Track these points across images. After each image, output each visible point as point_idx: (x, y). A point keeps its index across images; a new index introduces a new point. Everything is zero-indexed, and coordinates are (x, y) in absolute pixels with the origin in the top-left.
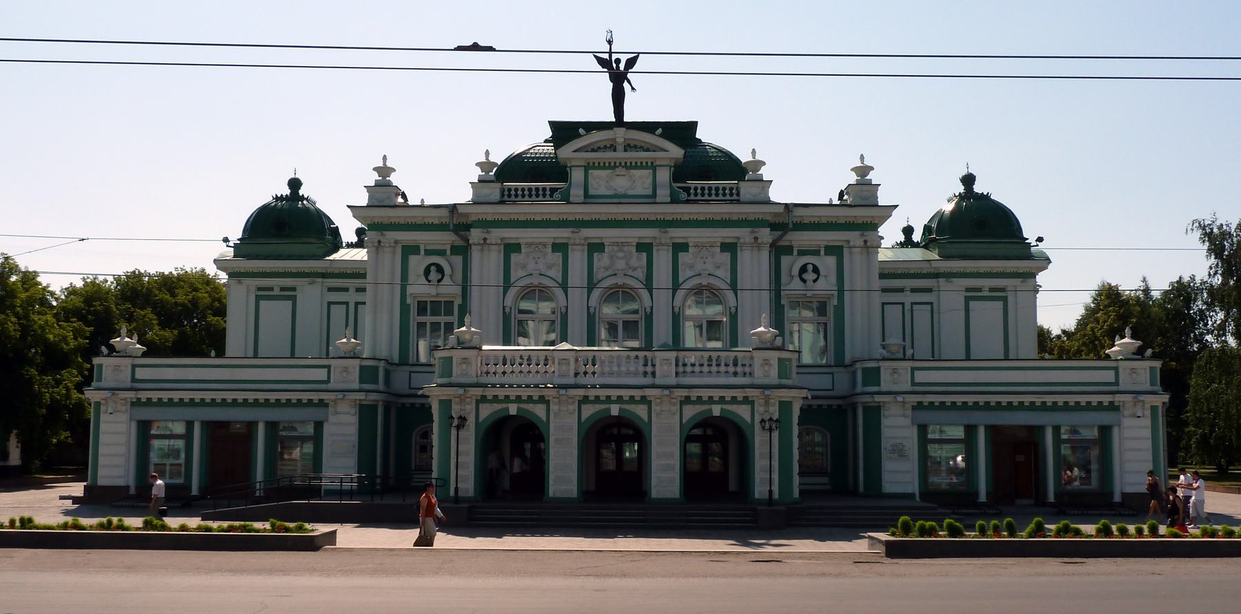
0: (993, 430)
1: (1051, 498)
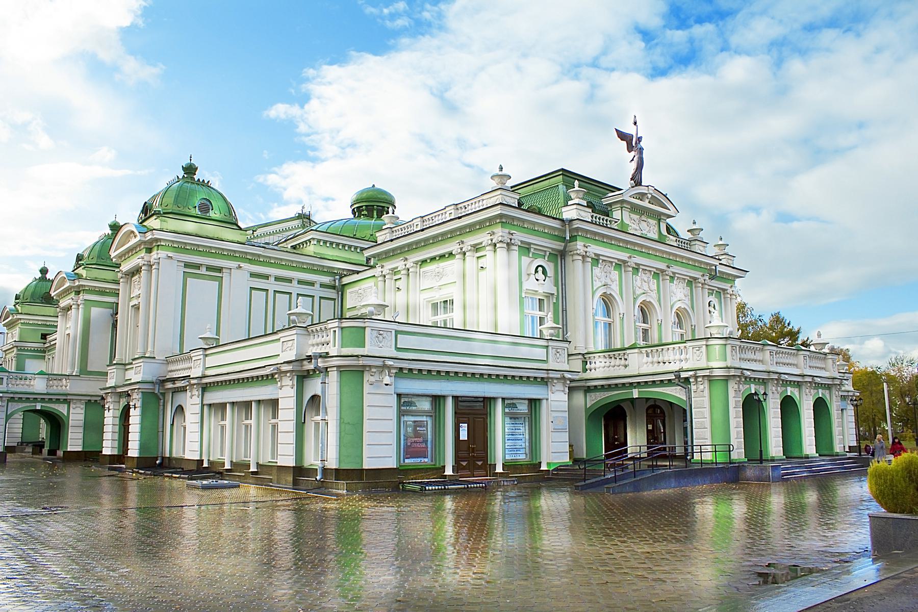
0: (455, 398)
1: (499, 469)
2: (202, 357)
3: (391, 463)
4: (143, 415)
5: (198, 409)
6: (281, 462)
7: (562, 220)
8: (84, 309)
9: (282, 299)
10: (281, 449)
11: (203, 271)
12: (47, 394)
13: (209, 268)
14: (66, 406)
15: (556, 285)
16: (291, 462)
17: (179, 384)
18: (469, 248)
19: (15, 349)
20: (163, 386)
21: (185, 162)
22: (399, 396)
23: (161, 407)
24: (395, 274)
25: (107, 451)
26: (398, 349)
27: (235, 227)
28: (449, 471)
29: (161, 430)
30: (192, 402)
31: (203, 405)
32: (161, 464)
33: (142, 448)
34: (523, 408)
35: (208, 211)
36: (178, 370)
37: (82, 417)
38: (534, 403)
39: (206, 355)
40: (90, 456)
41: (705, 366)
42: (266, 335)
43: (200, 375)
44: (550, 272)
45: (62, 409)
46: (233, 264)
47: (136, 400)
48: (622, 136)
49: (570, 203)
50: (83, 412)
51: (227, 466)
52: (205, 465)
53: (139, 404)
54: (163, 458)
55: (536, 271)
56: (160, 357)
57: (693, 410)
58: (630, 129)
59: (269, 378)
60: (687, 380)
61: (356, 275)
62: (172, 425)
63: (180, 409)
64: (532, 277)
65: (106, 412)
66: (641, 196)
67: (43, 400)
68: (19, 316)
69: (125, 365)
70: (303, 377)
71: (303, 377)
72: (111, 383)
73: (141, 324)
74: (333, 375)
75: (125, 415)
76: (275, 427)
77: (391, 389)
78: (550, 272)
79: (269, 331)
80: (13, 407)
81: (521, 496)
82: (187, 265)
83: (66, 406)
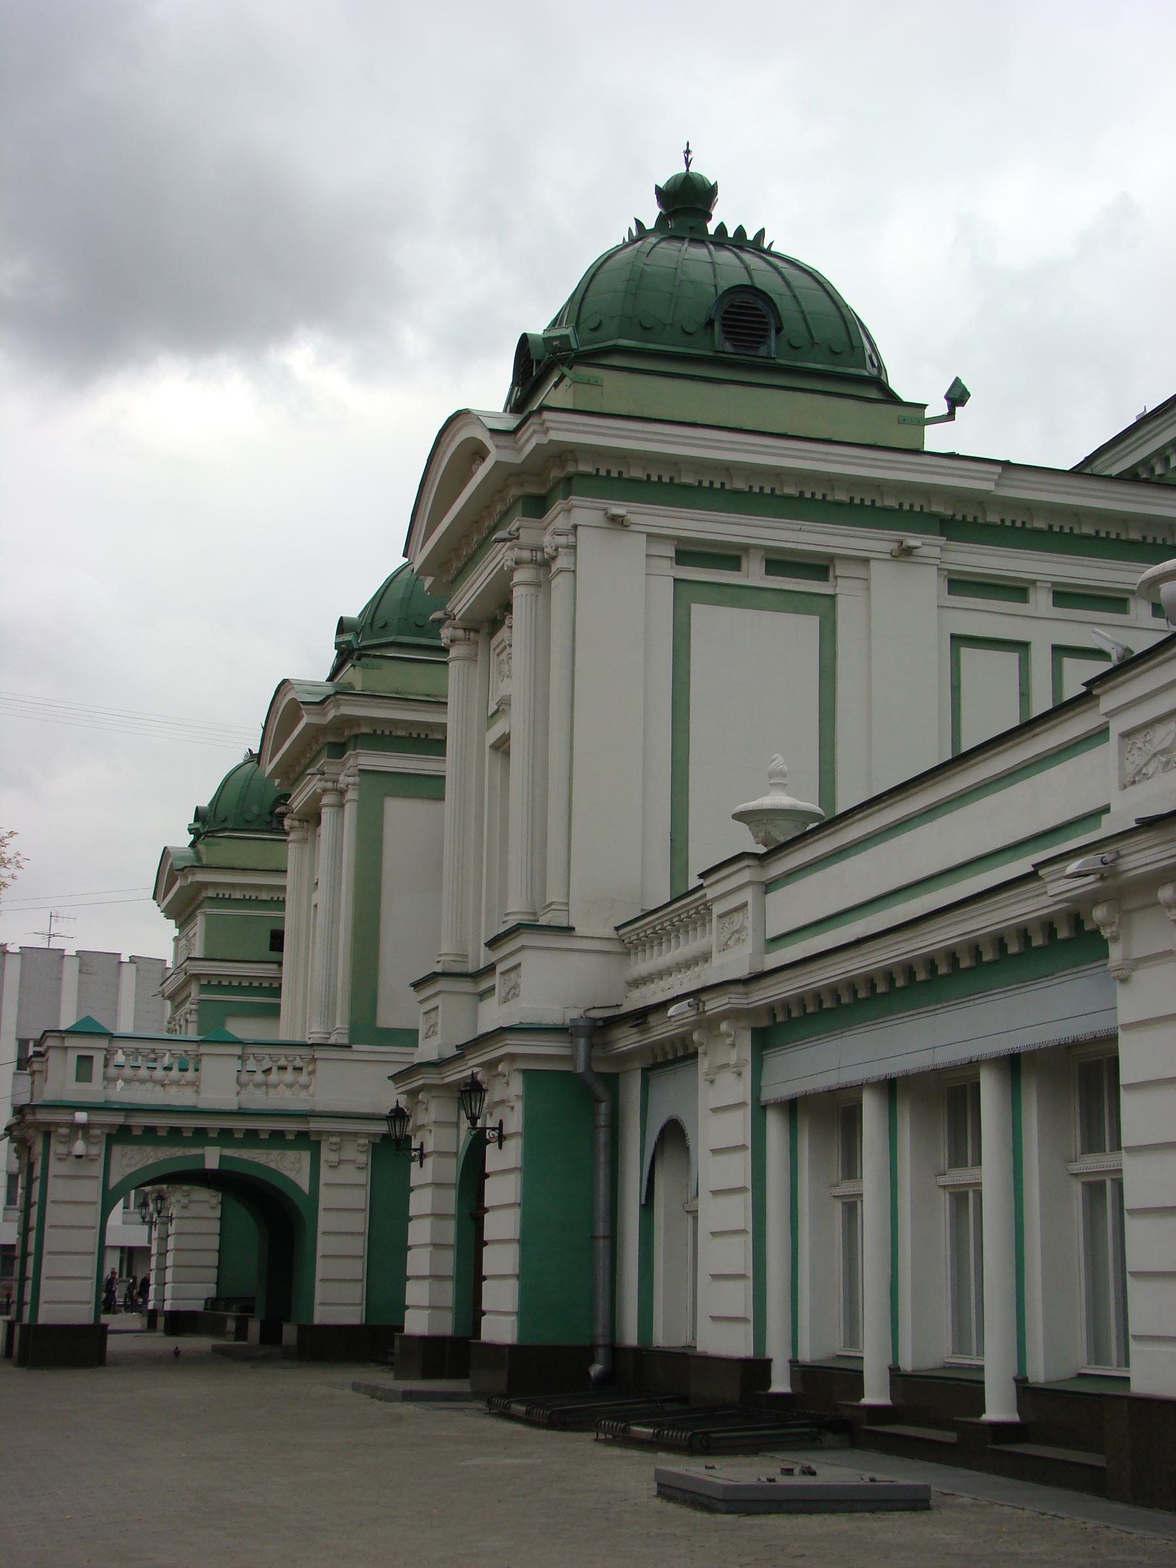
2: (747, 895)
4: (533, 1170)
5: (738, 1128)
8: (361, 803)
11: (753, 574)
12: (241, 1113)
13: (778, 563)
14: (306, 1156)
19: (194, 989)
20: (605, 1045)
21: (668, 170)
23: (602, 1136)
25: (416, 1323)
27: (874, 394)
29: (602, 1229)
30: (718, 1104)
31: (760, 1110)
32: (607, 1378)
33: (526, 1312)
35: (763, 338)
37: (361, 1198)
39: (769, 886)
40: (373, 1342)
42: (1028, 727)
45: (292, 1167)
46: (872, 541)
50: (364, 1177)
52: (780, 1384)
53: (514, 1122)
54: (616, 1351)
56: (594, 924)
62: (647, 1206)
63: (674, 1136)
65: (415, 1166)
67: (226, 1137)
68: (202, 877)
79: (1041, 703)
81: (186, 920)
82: (688, 553)
83: (306, 1156)
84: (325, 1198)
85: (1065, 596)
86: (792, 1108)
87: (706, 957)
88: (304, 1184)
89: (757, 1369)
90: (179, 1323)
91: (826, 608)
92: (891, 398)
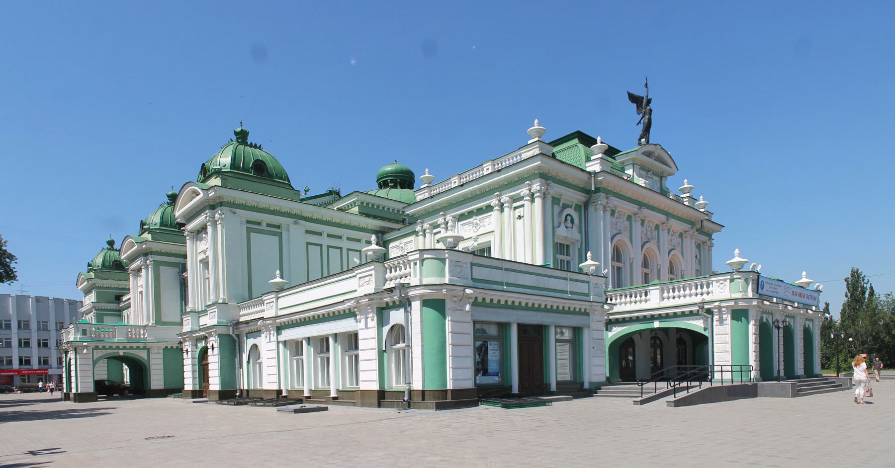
0: (522, 328)
1: (553, 387)
3: (162, 387)
6: (363, 386)
7: (589, 173)
9: (334, 253)
10: (362, 376)
15: (580, 232)
16: (375, 387)
17: (252, 328)
18: (507, 199)
22: (475, 322)
24: (435, 228)
26: (474, 280)
28: (515, 390)
31: (278, 343)
33: (223, 382)
34: (567, 334)
36: (247, 314)
38: (577, 331)
41: (728, 297)
43: (274, 315)
44: (576, 221)
47: (214, 341)
48: (633, 98)
49: (592, 158)
51: (306, 394)
52: (284, 394)
54: (241, 391)
55: (566, 220)
57: (715, 337)
58: (640, 92)
59: (350, 314)
60: (709, 311)
61: (397, 232)
62: (248, 362)
64: (563, 226)
65: (185, 354)
66: (649, 154)
67: (660, 317)
69: (199, 312)
70: (382, 313)
71: (382, 313)
72: (187, 328)
73: (211, 276)
74: (416, 305)
75: (204, 353)
76: (357, 357)
77: (469, 318)
78: (576, 221)
80: (98, 354)
84: (152, 362)
85: (329, 236)
86: (285, 343)
87: (264, 311)
88: (146, 358)
89: (279, 392)
90: (81, 397)
91: (280, 235)
92: (293, 189)
